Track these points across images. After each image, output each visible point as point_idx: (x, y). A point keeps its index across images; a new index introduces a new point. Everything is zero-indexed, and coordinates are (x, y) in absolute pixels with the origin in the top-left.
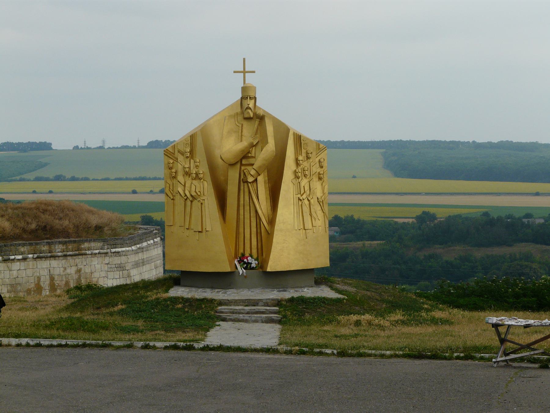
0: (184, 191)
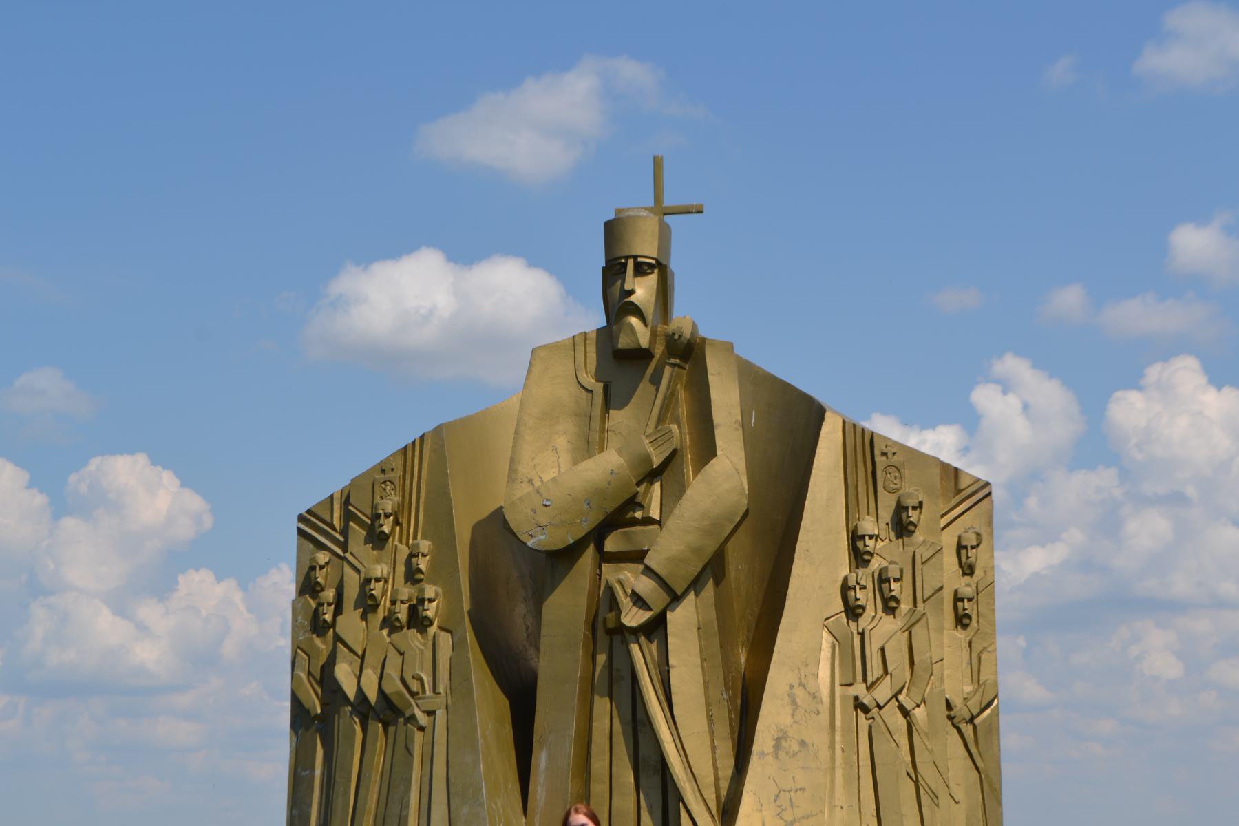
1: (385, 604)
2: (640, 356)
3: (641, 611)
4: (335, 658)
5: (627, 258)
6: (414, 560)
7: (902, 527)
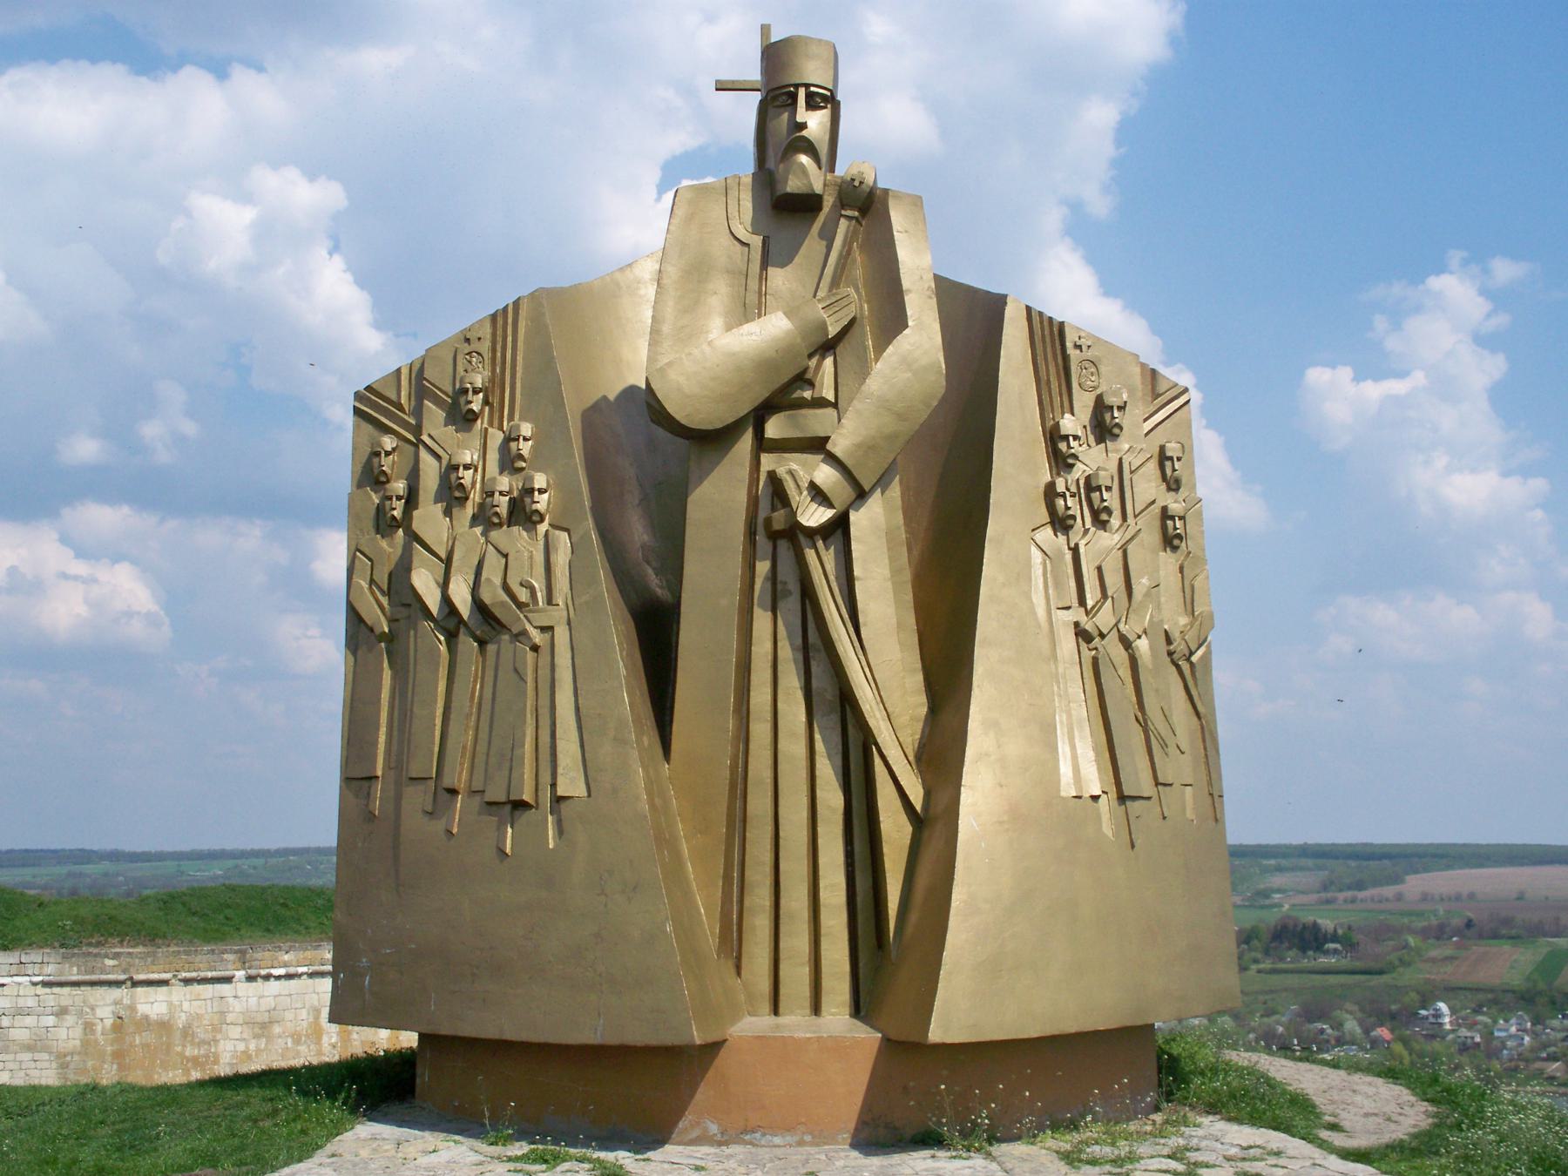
0: (445, 586)
1: (475, 496)
2: (802, 207)
3: (822, 509)
4: (410, 562)
5: (797, 86)
6: (513, 445)
7: (1103, 428)
